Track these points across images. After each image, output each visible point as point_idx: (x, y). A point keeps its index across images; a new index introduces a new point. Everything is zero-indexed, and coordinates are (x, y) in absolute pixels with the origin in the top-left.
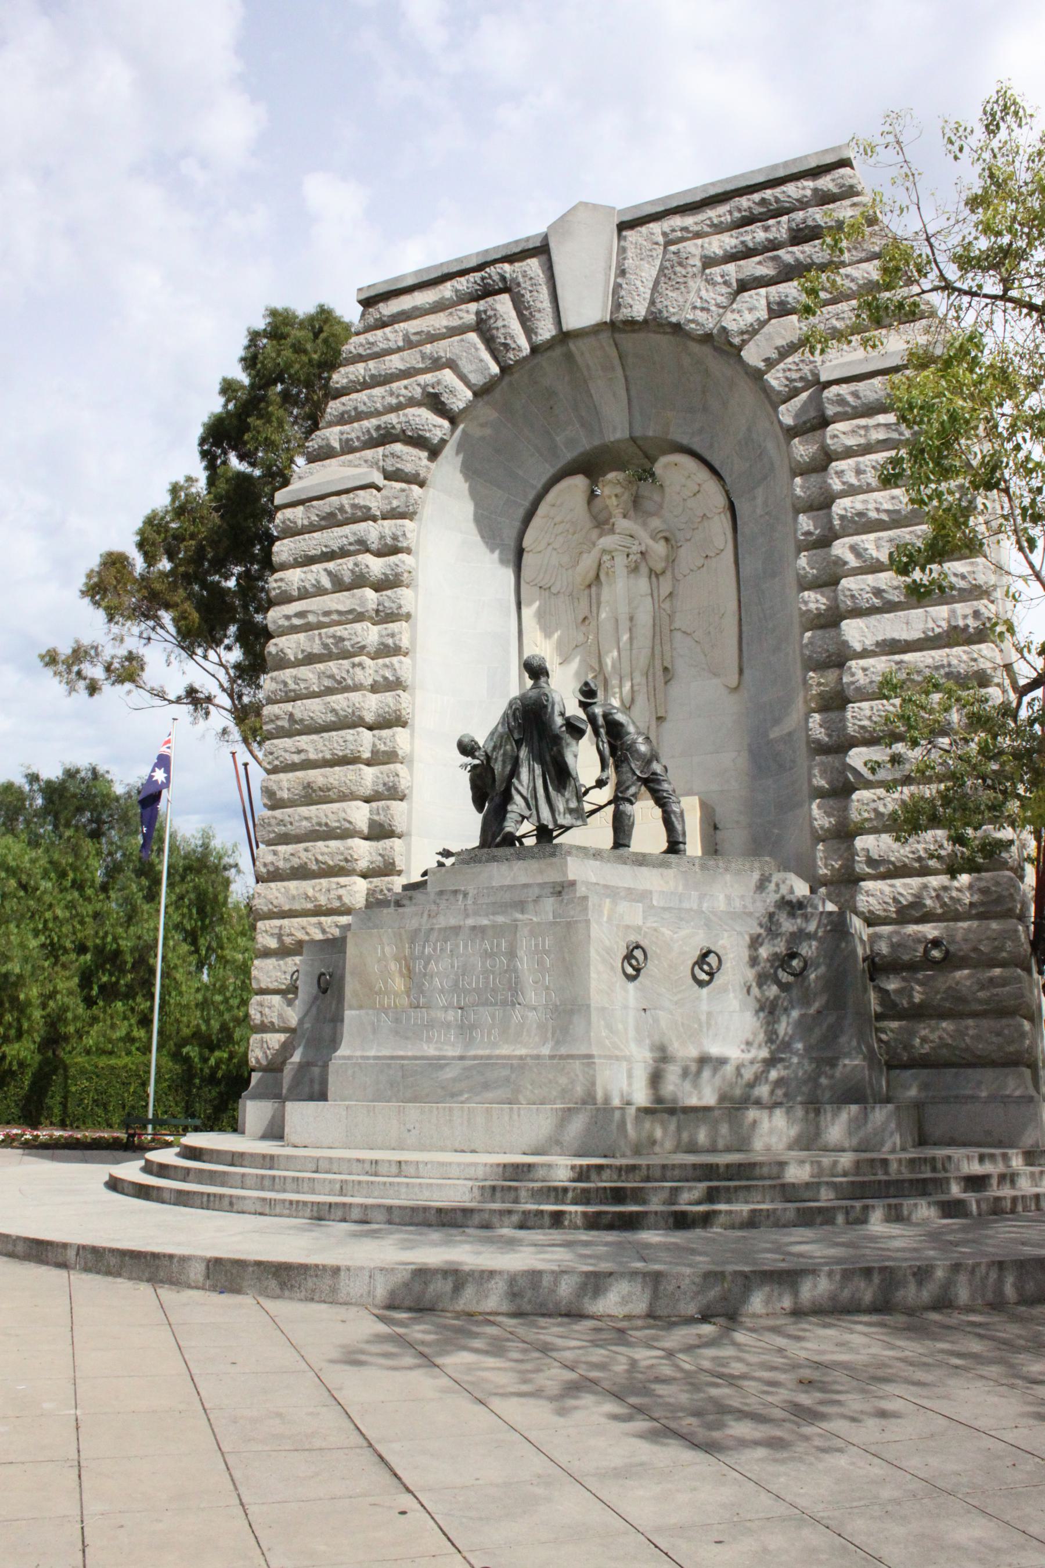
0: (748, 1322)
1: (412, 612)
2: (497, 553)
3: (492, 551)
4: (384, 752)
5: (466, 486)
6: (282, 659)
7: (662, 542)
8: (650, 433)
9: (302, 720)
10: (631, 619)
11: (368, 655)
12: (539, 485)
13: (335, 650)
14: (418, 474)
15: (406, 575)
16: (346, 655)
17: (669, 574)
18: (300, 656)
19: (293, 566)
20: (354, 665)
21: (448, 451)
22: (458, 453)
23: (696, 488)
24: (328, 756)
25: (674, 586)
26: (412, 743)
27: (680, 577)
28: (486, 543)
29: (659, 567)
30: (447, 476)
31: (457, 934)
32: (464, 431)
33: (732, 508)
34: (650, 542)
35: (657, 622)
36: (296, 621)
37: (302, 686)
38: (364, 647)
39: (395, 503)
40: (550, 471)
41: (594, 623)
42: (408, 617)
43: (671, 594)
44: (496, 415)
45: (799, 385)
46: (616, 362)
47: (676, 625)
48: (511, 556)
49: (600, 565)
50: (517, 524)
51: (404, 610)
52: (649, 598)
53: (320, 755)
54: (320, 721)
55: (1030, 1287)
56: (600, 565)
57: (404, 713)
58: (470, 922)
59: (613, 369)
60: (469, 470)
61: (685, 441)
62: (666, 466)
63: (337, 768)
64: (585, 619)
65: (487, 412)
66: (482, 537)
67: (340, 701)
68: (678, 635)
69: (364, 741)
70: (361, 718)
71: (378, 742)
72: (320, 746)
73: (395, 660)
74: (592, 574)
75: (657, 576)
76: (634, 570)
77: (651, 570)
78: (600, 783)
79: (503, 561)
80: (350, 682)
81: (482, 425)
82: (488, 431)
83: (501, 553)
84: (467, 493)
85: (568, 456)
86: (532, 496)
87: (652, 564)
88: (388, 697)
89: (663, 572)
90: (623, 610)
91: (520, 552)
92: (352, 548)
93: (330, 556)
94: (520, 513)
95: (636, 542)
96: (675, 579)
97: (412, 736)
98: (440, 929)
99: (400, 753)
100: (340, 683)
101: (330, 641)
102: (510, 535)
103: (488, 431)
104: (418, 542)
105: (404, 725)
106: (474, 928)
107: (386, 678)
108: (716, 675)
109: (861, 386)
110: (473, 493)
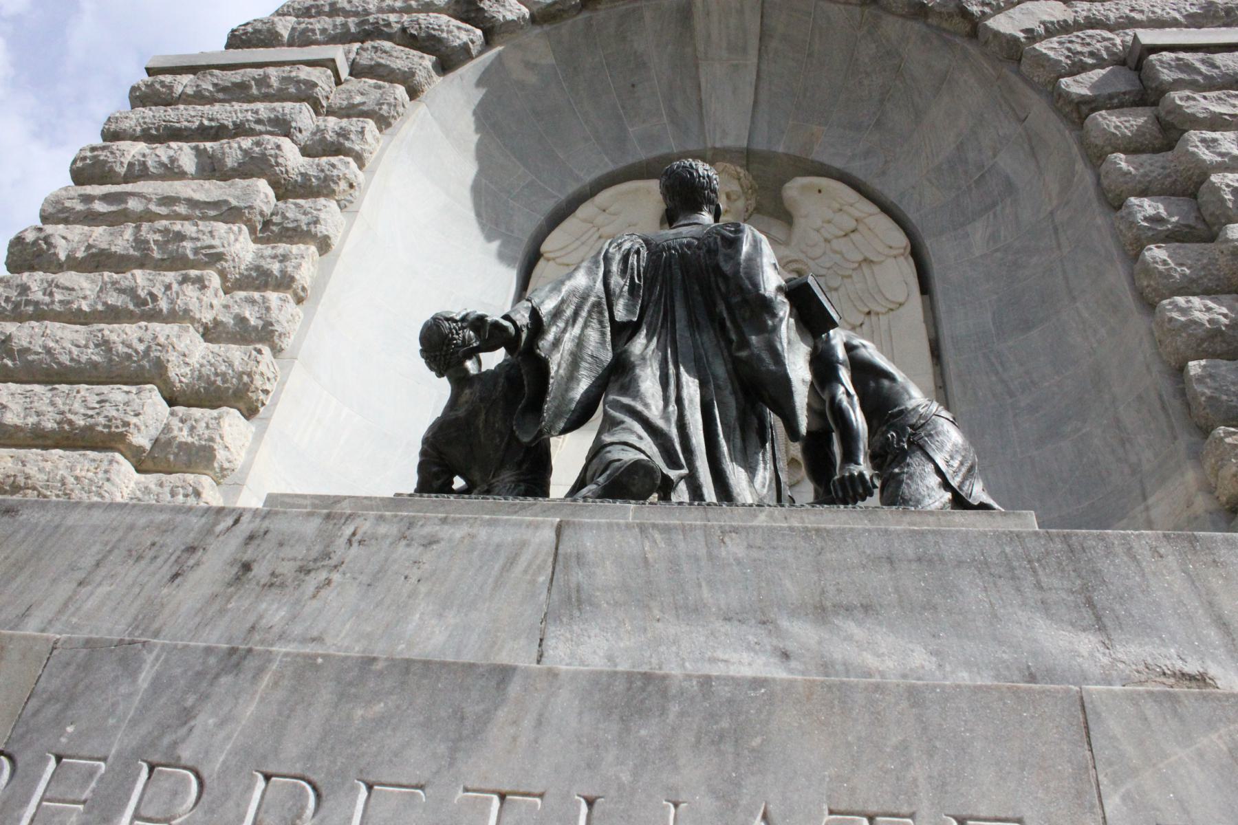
1: (335, 242)
2: (495, 245)
3: (489, 238)
4: (183, 446)
5: (475, 138)
6: (39, 254)
8: (781, 149)
9: (25, 351)
11: (223, 274)
12: (588, 178)
13: (156, 255)
14: (413, 74)
15: (343, 185)
16: (176, 262)
18: (80, 254)
19: (135, 138)
20: (185, 280)
21: (469, 71)
22: (480, 83)
23: (853, 224)
24: (50, 425)
26: (252, 452)
28: (482, 226)
30: (451, 103)
31: (464, 734)
32: (499, 55)
33: (917, 254)
36: (100, 207)
37: (58, 297)
38: (220, 257)
39: (358, 99)
40: (607, 166)
42: (324, 245)
44: (550, 60)
45: (1090, 61)
46: (754, 42)
48: (520, 253)
50: (539, 219)
51: (321, 229)
53: (32, 420)
54: (65, 359)
57: (258, 382)
58: (587, 649)
59: (744, 50)
60: (485, 116)
61: (838, 163)
62: (804, 188)
63: (57, 452)
65: (538, 45)
66: (478, 215)
67: (127, 336)
69: (148, 414)
70: (160, 367)
71: (175, 423)
72: (43, 406)
73: (273, 297)
79: (502, 256)
80: (164, 305)
82: (532, 78)
83: (502, 245)
84: (473, 147)
85: (640, 154)
86: (572, 188)
88: (236, 353)
92: (258, 127)
93: (204, 133)
94: (548, 206)
97: (259, 437)
98: (306, 669)
99: (221, 455)
100: (141, 302)
101: (152, 237)
102: (527, 226)
103: (532, 78)
104: (379, 158)
105: (250, 412)
106: (635, 695)
107: (241, 320)
109: (1219, 58)
110: (482, 154)
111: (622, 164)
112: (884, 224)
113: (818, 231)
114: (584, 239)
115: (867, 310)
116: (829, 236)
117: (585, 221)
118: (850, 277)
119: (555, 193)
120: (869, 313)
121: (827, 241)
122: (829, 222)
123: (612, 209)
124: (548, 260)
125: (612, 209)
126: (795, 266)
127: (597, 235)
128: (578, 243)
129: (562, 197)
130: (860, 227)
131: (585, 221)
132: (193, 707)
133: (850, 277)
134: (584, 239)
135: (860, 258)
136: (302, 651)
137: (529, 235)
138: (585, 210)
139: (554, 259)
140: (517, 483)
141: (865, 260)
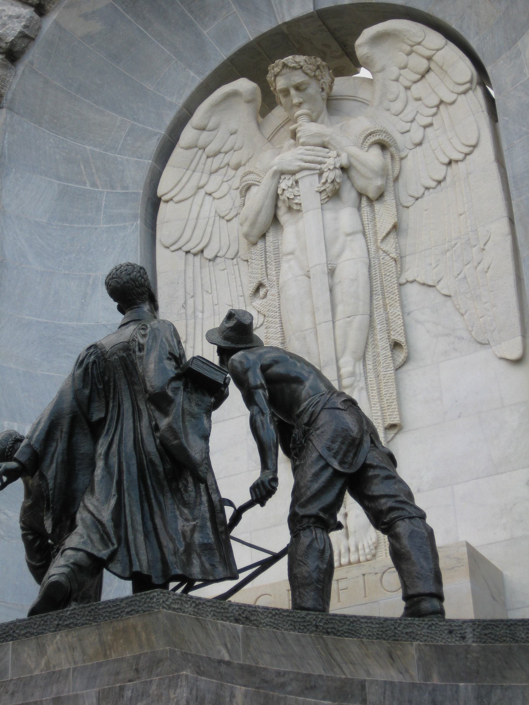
0: (329, 215)
7: (376, 151)
10: (332, 272)
17: (389, 198)
23: (424, 64)
25: (399, 215)
27: (406, 200)
29: (372, 186)
34: (355, 150)
35: (377, 284)
41: (273, 291)
43: (395, 227)
47: (408, 275)
49: (277, 196)
50: (148, 162)
52: (360, 236)
55: (220, 570)
56: (277, 196)
64: (260, 286)
68: (413, 292)
74: (265, 217)
75: (370, 201)
76: (334, 195)
77: (360, 195)
78: (262, 492)
81: (86, 16)
85: (220, 54)
87: (360, 183)
89: (381, 196)
90: (317, 259)
91: (154, 203)
94: (153, 146)
95: (333, 153)
96: (400, 206)
108: (483, 344)
111: (208, 72)
112: (452, 52)
113: (397, 80)
114: (192, 167)
115: (446, 161)
116: (408, 84)
117: (188, 148)
118: (431, 125)
119: (156, 130)
120: (450, 163)
121: (408, 88)
122: (405, 67)
123: (211, 125)
124: (167, 202)
125: (211, 125)
126: (373, 139)
127: (204, 156)
128: (189, 172)
129: (163, 132)
130: (433, 66)
131: (188, 148)
132: (210, 117)
133: (431, 125)
134: (192, 167)
135: (437, 102)
136: (65, 429)
137: (142, 184)
138: (188, 135)
139: (171, 200)
140: (299, 380)
141: (442, 102)
